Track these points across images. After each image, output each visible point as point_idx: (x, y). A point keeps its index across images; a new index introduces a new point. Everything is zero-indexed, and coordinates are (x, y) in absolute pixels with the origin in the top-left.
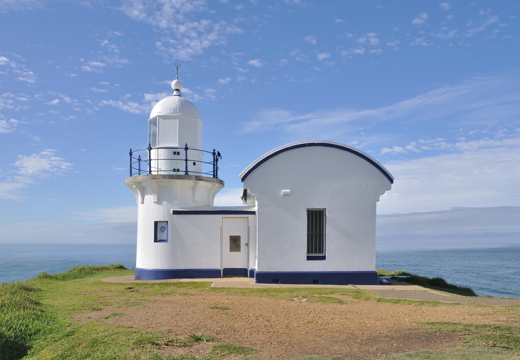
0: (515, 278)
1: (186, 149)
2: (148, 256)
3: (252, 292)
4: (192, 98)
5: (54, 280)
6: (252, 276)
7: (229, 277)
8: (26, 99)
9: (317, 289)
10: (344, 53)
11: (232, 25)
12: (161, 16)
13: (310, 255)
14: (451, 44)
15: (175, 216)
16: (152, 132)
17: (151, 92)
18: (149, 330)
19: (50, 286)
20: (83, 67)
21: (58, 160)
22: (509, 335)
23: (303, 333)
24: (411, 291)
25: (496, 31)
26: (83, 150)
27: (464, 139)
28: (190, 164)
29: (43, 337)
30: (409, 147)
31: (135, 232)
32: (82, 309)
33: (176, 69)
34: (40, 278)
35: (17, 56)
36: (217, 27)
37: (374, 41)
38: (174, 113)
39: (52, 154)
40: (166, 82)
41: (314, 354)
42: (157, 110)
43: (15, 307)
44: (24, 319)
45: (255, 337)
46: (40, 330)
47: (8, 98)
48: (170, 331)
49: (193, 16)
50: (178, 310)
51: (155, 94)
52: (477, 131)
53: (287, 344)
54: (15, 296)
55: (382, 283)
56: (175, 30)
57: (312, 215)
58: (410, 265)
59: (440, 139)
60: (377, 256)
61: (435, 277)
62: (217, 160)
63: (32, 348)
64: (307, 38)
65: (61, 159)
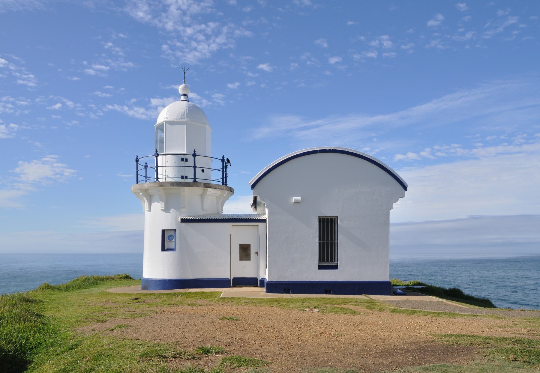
0: (536, 289)
1: (195, 155)
2: (156, 266)
3: (262, 302)
4: (201, 104)
5: (56, 290)
6: (262, 285)
7: (239, 287)
8: (26, 103)
9: (329, 299)
10: (356, 57)
11: (241, 28)
12: (167, 17)
13: (322, 264)
14: (467, 47)
15: (184, 224)
16: (159, 138)
17: (158, 96)
18: (156, 342)
19: (52, 297)
20: (87, 70)
21: (61, 167)
22: (530, 349)
23: (315, 344)
24: (426, 302)
25: (516, 32)
26: (87, 156)
27: (481, 144)
28: (199, 171)
29: (45, 351)
30: (423, 154)
31: (142, 241)
32: (86, 321)
33: (184, 73)
34: (42, 289)
35: (16, 58)
36: (225, 30)
37: (387, 44)
38: (182, 118)
39: (55, 160)
40: (173, 86)
41: (326, 366)
42: (163, 116)
43: (14, 320)
44: (24, 332)
45: (266, 348)
46: (41, 344)
47: (7, 102)
48: (178, 343)
49: (200, 18)
50: (186, 321)
51: (162, 99)
52: (495, 136)
53: (298, 356)
54: (15, 308)
55: (396, 294)
56: (182, 33)
57: (324, 223)
58: (425, 275)
59: (456, 145)
60: (391, 266)
61: (452, 287)
62: (226, 167)
63: (33, 362)
64: (318, 42)
65: (64, 165)
